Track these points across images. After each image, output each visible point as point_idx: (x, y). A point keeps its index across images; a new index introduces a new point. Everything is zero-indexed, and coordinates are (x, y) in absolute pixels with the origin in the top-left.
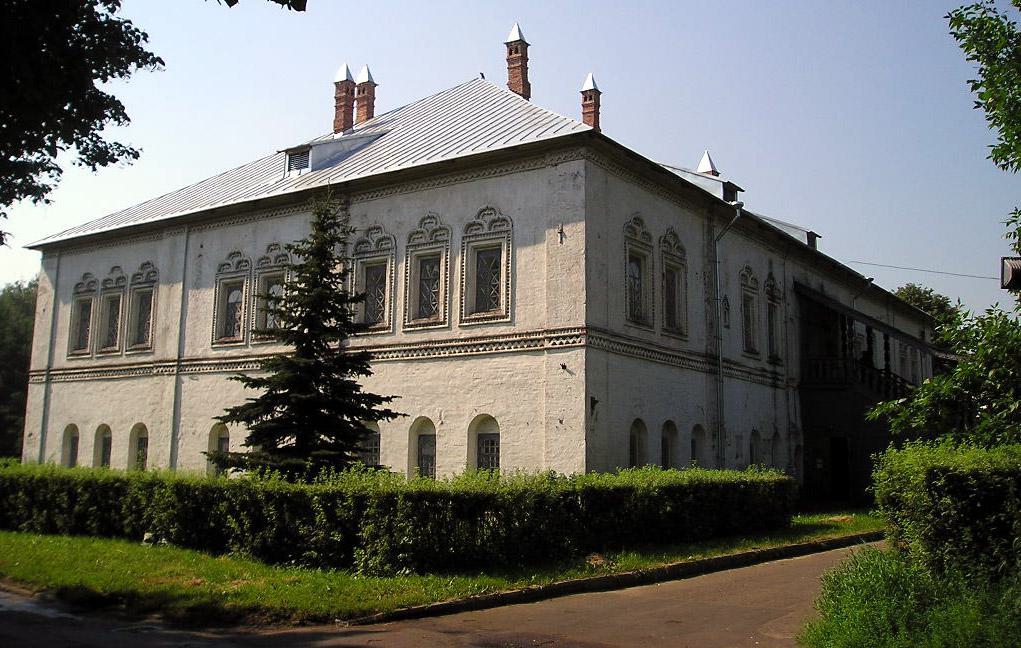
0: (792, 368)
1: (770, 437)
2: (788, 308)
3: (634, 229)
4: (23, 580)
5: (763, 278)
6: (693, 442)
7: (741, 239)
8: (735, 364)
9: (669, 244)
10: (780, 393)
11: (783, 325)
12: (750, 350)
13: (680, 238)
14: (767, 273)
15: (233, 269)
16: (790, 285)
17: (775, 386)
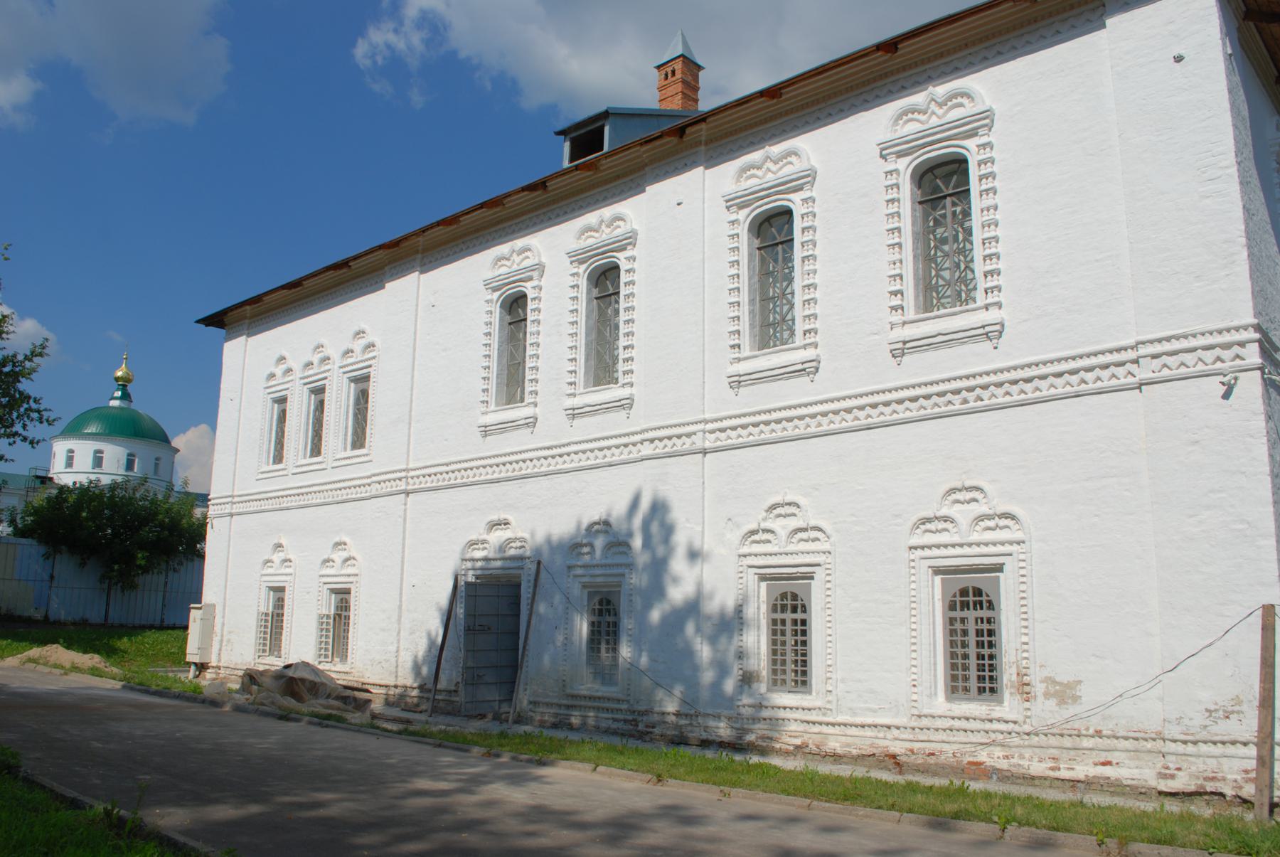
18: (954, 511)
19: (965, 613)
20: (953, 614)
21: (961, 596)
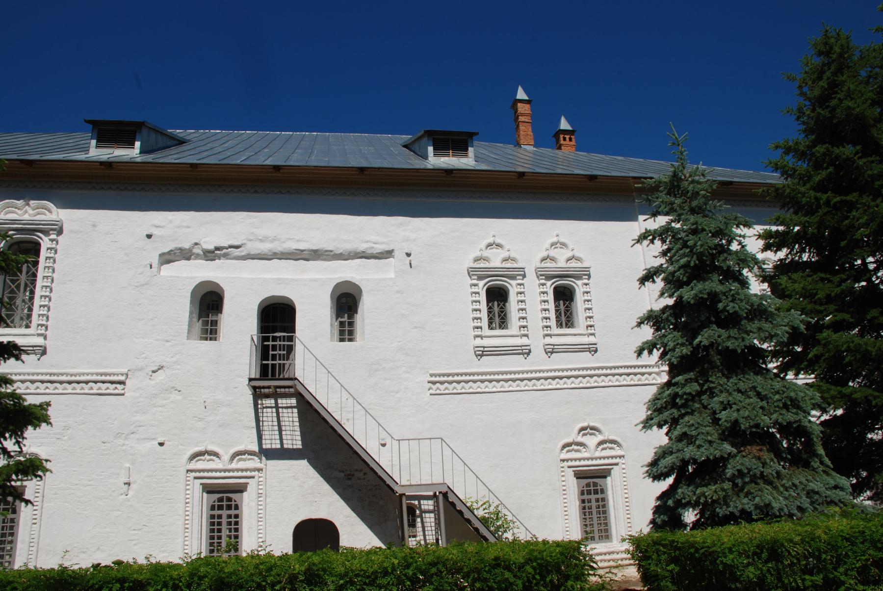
18: (586, 440)
19: (589, 497)
20: (213, 512)
21: (218, 502)
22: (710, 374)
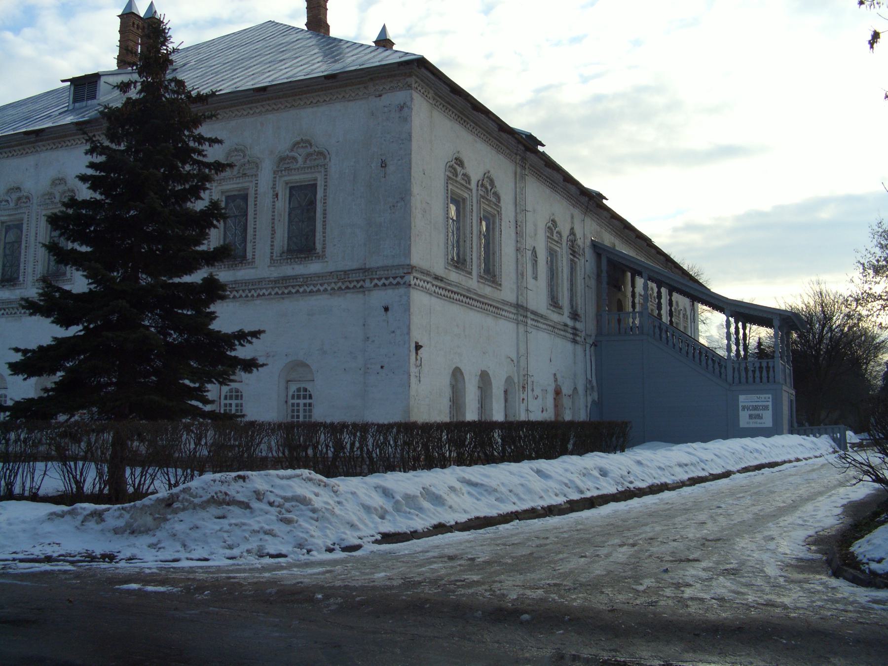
0: (587, 325)
1: (570, 392)
2: (587, 264)
3: (455, 169)
4: (310, 621)
5: (566, 233)
6: (506, 392)
7: (548, 191)
8: (542, 316)
9: (486, 189)
10: (579, 348)
11: (583, 281)
12: (555, 303)
13: (496, 184)
14: (570, 228)
15: (12, 205)
16: (588, 242)
17: (575, 342)
22: (165, 52)
